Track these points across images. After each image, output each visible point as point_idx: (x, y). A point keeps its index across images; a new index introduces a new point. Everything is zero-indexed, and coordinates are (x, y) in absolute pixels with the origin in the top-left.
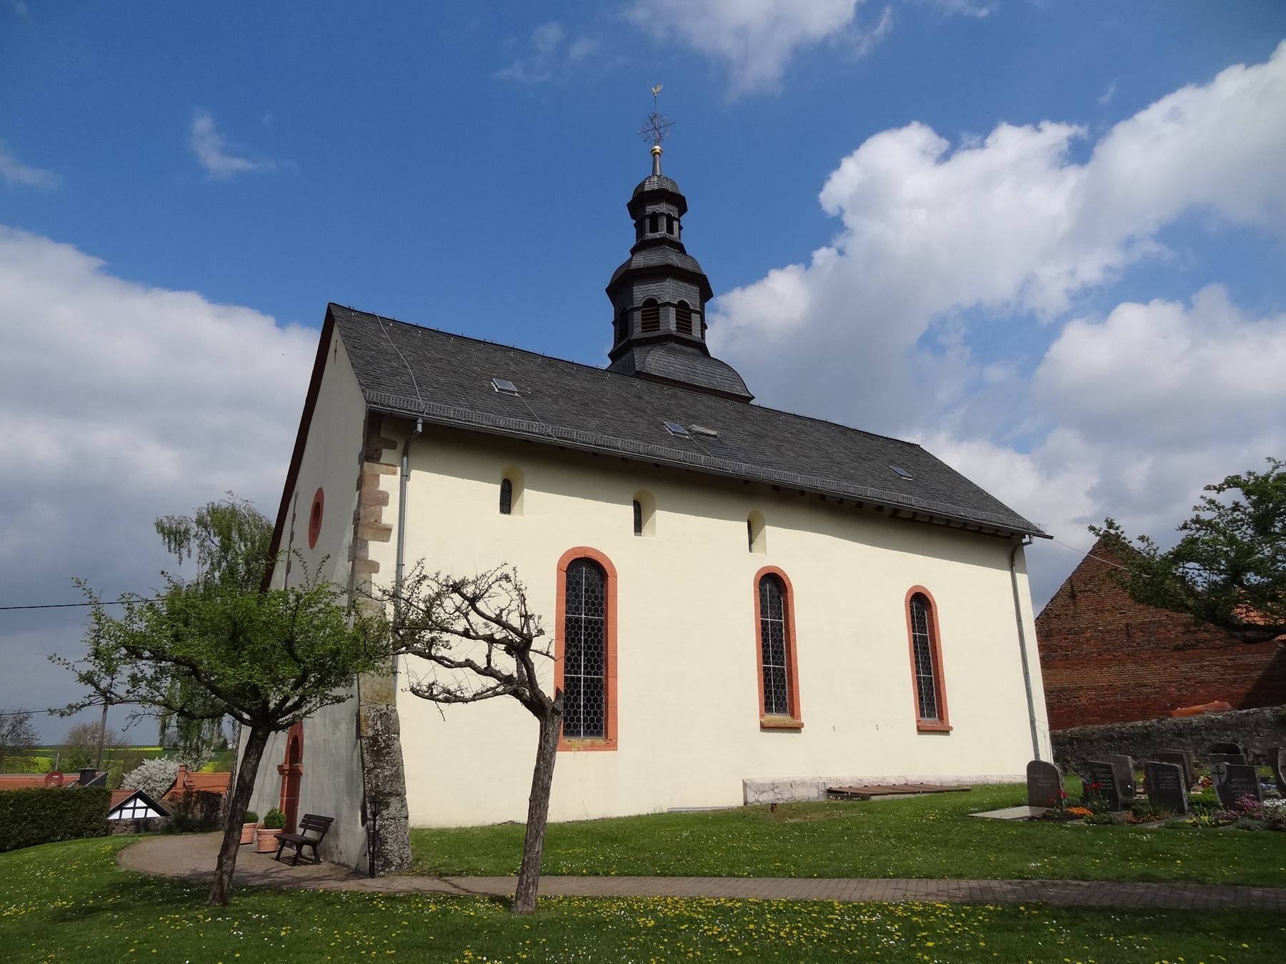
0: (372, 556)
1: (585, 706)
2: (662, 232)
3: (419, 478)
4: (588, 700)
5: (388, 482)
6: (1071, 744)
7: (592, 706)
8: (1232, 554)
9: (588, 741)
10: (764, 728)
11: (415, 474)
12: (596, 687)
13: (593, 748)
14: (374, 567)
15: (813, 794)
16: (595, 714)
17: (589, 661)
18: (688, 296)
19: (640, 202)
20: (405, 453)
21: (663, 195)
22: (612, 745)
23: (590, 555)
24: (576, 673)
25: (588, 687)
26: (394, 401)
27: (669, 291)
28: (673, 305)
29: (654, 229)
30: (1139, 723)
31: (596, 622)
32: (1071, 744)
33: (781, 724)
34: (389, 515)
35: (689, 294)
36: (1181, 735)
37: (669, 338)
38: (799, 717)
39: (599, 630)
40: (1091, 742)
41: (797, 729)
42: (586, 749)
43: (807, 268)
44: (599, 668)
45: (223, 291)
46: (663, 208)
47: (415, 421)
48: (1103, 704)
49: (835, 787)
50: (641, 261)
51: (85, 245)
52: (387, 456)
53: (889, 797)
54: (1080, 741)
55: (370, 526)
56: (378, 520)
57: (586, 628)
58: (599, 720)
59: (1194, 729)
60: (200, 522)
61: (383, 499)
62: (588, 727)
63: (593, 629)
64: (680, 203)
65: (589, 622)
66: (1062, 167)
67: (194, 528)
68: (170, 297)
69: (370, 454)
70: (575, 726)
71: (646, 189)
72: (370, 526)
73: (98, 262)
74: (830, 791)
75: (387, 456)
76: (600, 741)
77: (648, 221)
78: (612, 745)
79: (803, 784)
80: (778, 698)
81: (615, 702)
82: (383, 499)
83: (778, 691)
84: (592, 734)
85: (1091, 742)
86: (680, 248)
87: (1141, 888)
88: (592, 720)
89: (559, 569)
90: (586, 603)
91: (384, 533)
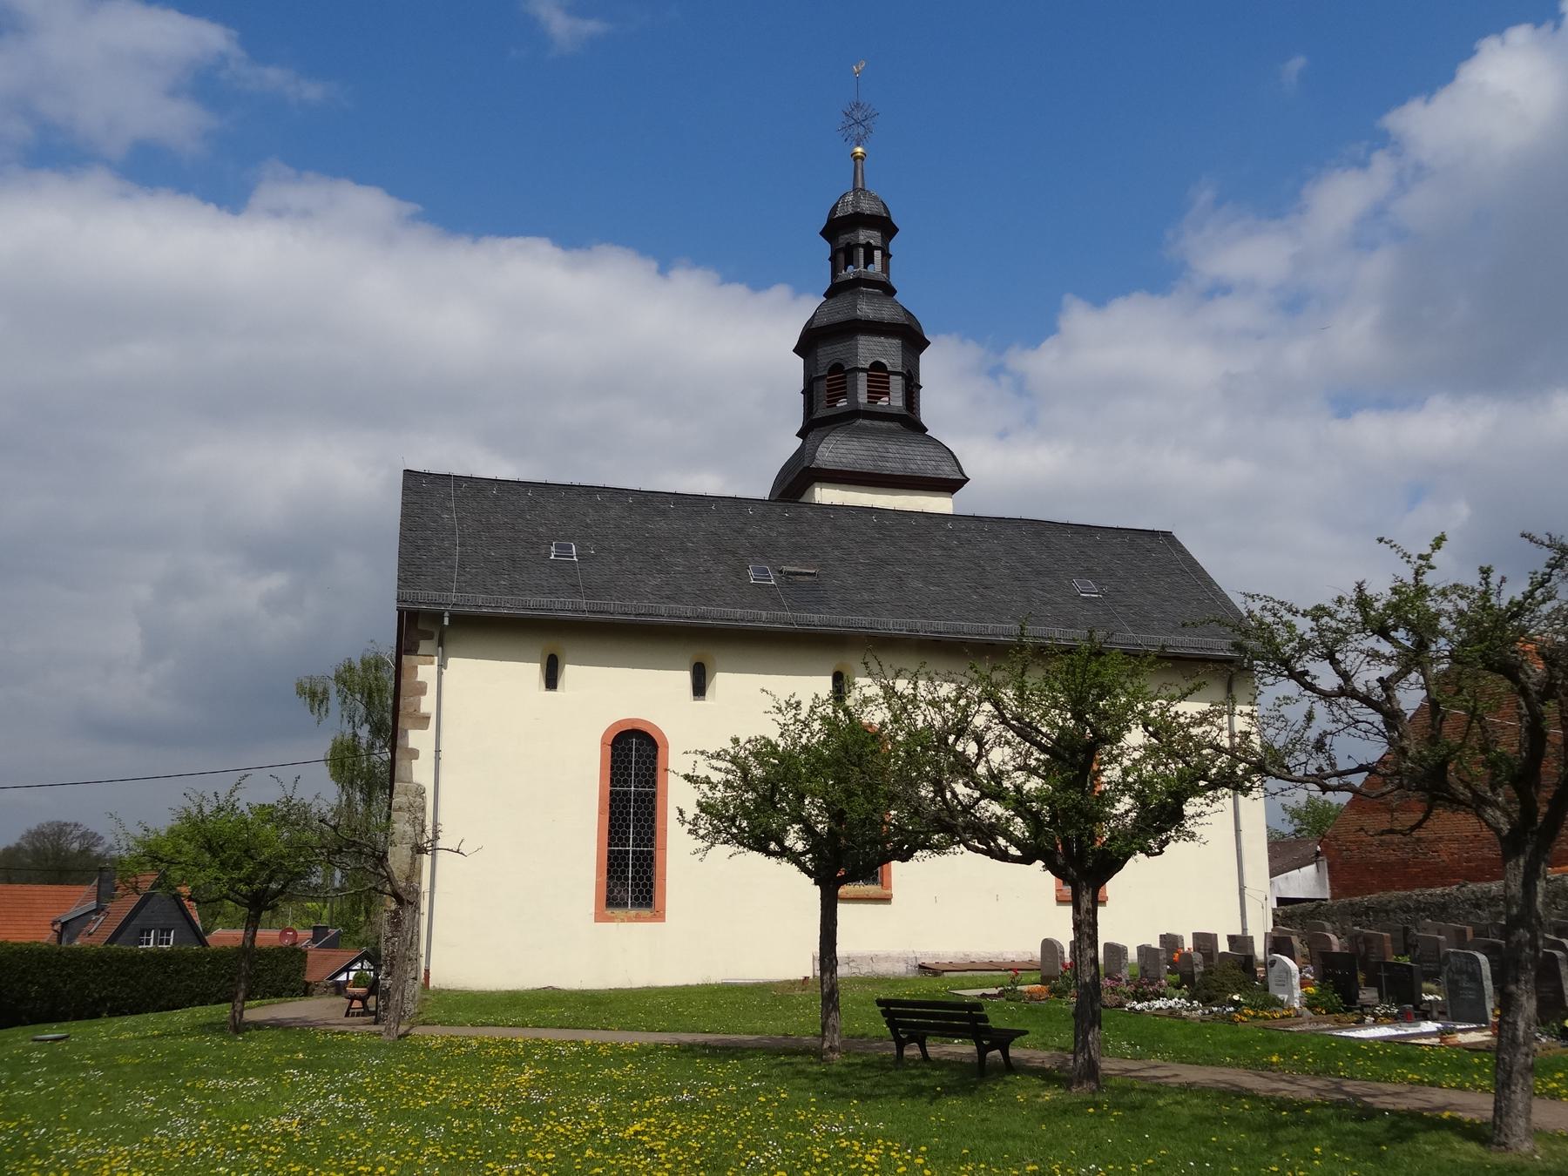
0: (412, 744)
1: (634, 879)
2: (876, 267)
3: (459, 667)
4: (637, 872)
5: (426, 672)
6: (1367, 915)
7: (641, 879)
8: (1410, 697)
9: (633, 912)
11: (452, 661)
12: (645, 859)
13: (638, 919)
14: (414, 754)
15: (900, 969)
16: (645, 885)
17: (638, 833)
18: (884, 355)
19: (837, 228)
20: (441, 644)
21: (859, 220)
22: (659, 916)
23: (637, 726)
25: (638, 859)
26: (427, 597)
27: (869, 350)
28: (863, 370)
30: (1439, 891)
31: (647, 794)
32: (1367, 915)
33: (861, 894)
34: (427, 704)
35: (887, 351)
36: (1478, 906)
37: (854, 414)
38: (890, 887)
39: (651, 801)
40: (1387, 912)
41: (886, 900)
42: (630, 920)
43: (1557, 27)
44: (650, 840)
45: (574, 230)
46: (864, 236)
47: (440, 615)
48: (1468, 860)
49: (928, 961)
51: (395, 188)
52: (425, 646)
53: (969, 974)
54: (1376, 912)
55: (410, 715)
56: (417, 710)
57: (636, 801)
58: (649, 892)
59: (1492, 899)
60: (339, 678)
61: (421, 689)
62: (637, 899)
63: (643, 801)
64: (887, 228)
65: (640, 794)
67: (333, 689)
68: (504, 245)
71: (839, 214)
72: (410, 715)
73: (409, 208)
74: (922, 967)
75: (425, 646)
76: (645, 912)
77: (861, 250)
78: (659, 916)
79: (887, 958)
81: (664, 874)
82: (421, 689)
84: (640, 905)
85: (1387, 912)
86: (889, 291)
87: (1389, 1099)
88: (641, 892)
89: (603, 743)
90: (636, 775)
91: (422, 721)
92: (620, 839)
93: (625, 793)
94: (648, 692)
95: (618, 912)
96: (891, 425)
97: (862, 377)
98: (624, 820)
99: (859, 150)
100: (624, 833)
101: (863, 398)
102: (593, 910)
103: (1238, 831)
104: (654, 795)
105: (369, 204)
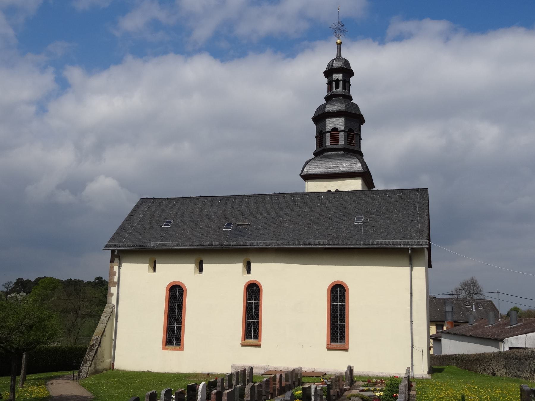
0: (112, 292)
10: (243, 345)
13: (175, 349)
22: (182, 349)
23: (180, 284)
24: (340, 300)
29: (337, 87)
33: (253, 344)
38: (260, 341)
41: (259, 346)
50: (330, 108)
62: (177, 342)
66: (447, 39)
69: (112, 261)
70: (341, 327)
76: (178, 347)
77: (334, 83)
78: (182, 349)
79: (68, 379)
80: (255, 333)
83: (252, 330)
84: (178, 345)
89: (167, 290)
91: (114, 284)
92: (172, 322)
93: (175, 306)
94: (180, 272)
95: (169, 347)
96: (339, 152)
97: (328, 135)
98: (174, 316)
99: (339, 41)
100: (174, 320)
101: (328, 144)
102: (161, 346)
103: (412, 321)
104: (182, 307)
105: (437, 26)
